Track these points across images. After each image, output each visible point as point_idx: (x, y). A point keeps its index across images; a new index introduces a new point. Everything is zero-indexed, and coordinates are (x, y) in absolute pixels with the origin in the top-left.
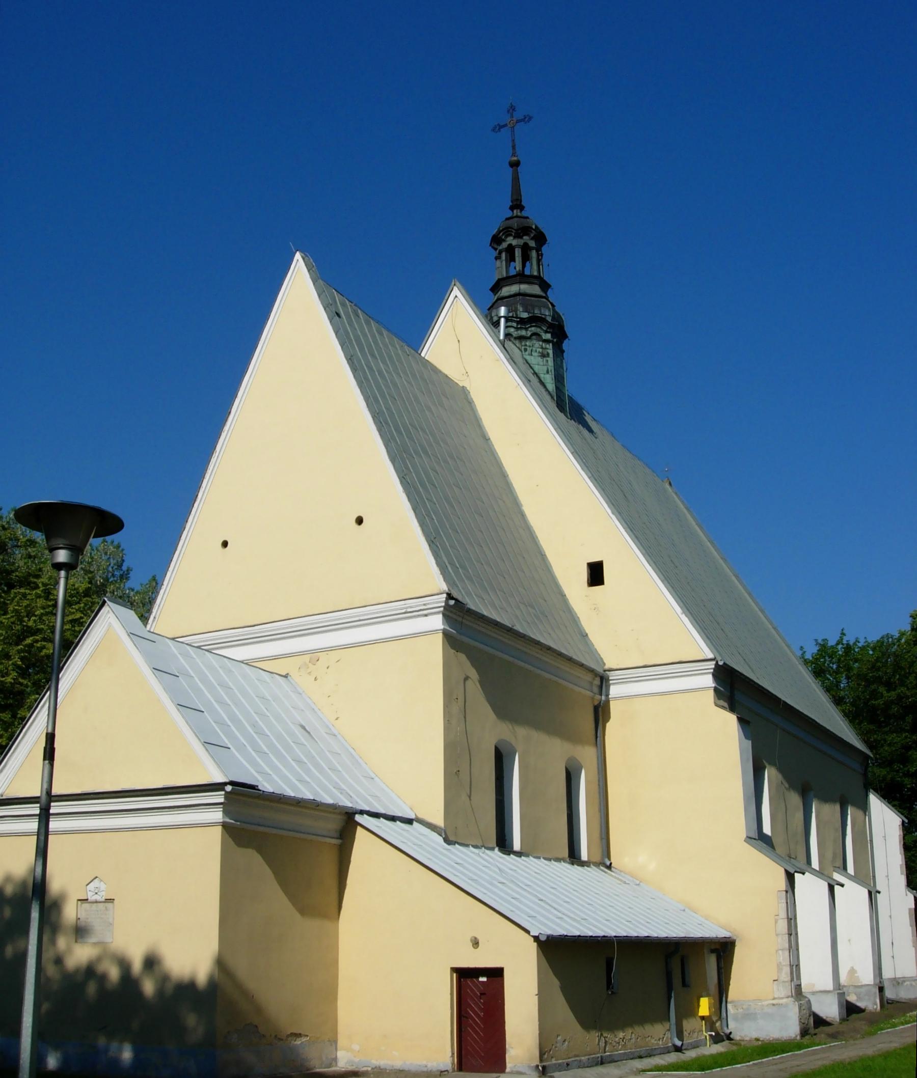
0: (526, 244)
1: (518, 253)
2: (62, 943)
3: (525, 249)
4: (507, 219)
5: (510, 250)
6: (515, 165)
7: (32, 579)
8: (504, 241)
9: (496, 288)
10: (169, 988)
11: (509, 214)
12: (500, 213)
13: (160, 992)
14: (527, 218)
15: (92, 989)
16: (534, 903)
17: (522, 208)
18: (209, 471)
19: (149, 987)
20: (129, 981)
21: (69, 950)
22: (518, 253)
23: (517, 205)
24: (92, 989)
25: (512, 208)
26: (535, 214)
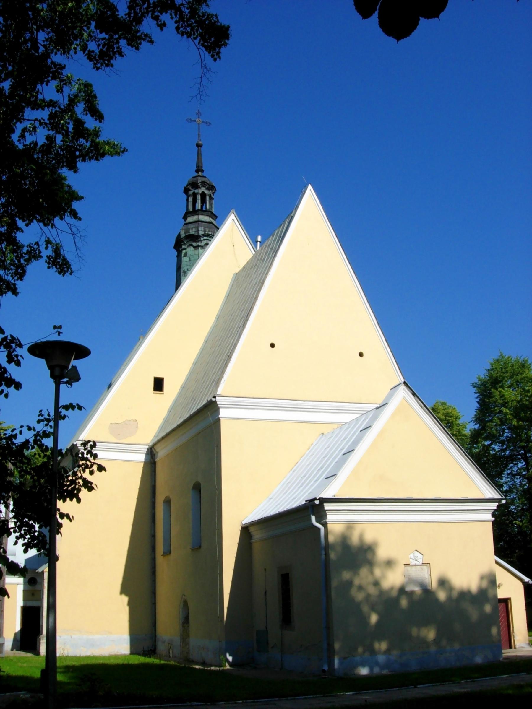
0: (203, 193)
1: (199, 197)
2: (378, 572)
3: (203, 195)
4: (193, 177)
5: (195, 195)
6: (199, 146)
7: (14, 345)
8: (200, 188)
9: (185, 218)
10: (455, 594)
11: (195, 174)
12: (190, 174)
13: (449, 598)
14: (205, 177)
15: (404, 602)
16: (303, 489)
17: (202, 171)
18: (327, 221)
19: (442, 596)
20: (427, 591)
21: (384, 576)
22: (199, 197)
23: (199, 169)
24: (404, 602)
25: (197, 171)
26: (210, 175)
